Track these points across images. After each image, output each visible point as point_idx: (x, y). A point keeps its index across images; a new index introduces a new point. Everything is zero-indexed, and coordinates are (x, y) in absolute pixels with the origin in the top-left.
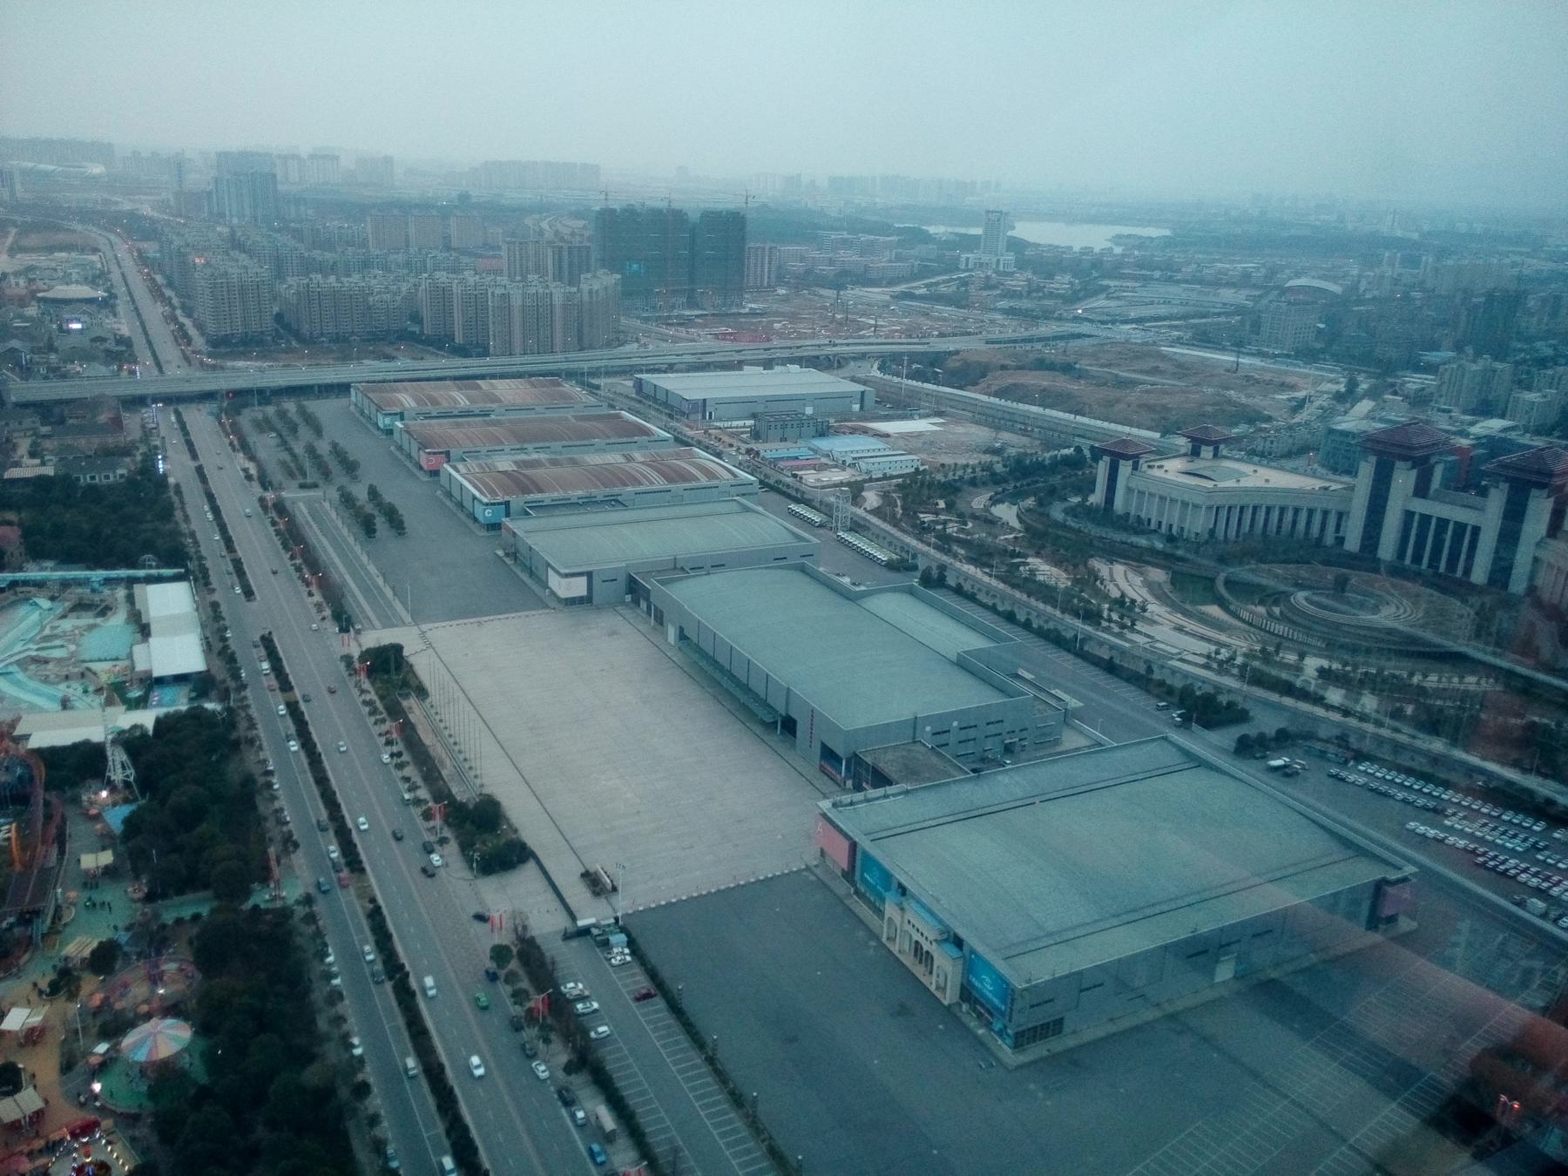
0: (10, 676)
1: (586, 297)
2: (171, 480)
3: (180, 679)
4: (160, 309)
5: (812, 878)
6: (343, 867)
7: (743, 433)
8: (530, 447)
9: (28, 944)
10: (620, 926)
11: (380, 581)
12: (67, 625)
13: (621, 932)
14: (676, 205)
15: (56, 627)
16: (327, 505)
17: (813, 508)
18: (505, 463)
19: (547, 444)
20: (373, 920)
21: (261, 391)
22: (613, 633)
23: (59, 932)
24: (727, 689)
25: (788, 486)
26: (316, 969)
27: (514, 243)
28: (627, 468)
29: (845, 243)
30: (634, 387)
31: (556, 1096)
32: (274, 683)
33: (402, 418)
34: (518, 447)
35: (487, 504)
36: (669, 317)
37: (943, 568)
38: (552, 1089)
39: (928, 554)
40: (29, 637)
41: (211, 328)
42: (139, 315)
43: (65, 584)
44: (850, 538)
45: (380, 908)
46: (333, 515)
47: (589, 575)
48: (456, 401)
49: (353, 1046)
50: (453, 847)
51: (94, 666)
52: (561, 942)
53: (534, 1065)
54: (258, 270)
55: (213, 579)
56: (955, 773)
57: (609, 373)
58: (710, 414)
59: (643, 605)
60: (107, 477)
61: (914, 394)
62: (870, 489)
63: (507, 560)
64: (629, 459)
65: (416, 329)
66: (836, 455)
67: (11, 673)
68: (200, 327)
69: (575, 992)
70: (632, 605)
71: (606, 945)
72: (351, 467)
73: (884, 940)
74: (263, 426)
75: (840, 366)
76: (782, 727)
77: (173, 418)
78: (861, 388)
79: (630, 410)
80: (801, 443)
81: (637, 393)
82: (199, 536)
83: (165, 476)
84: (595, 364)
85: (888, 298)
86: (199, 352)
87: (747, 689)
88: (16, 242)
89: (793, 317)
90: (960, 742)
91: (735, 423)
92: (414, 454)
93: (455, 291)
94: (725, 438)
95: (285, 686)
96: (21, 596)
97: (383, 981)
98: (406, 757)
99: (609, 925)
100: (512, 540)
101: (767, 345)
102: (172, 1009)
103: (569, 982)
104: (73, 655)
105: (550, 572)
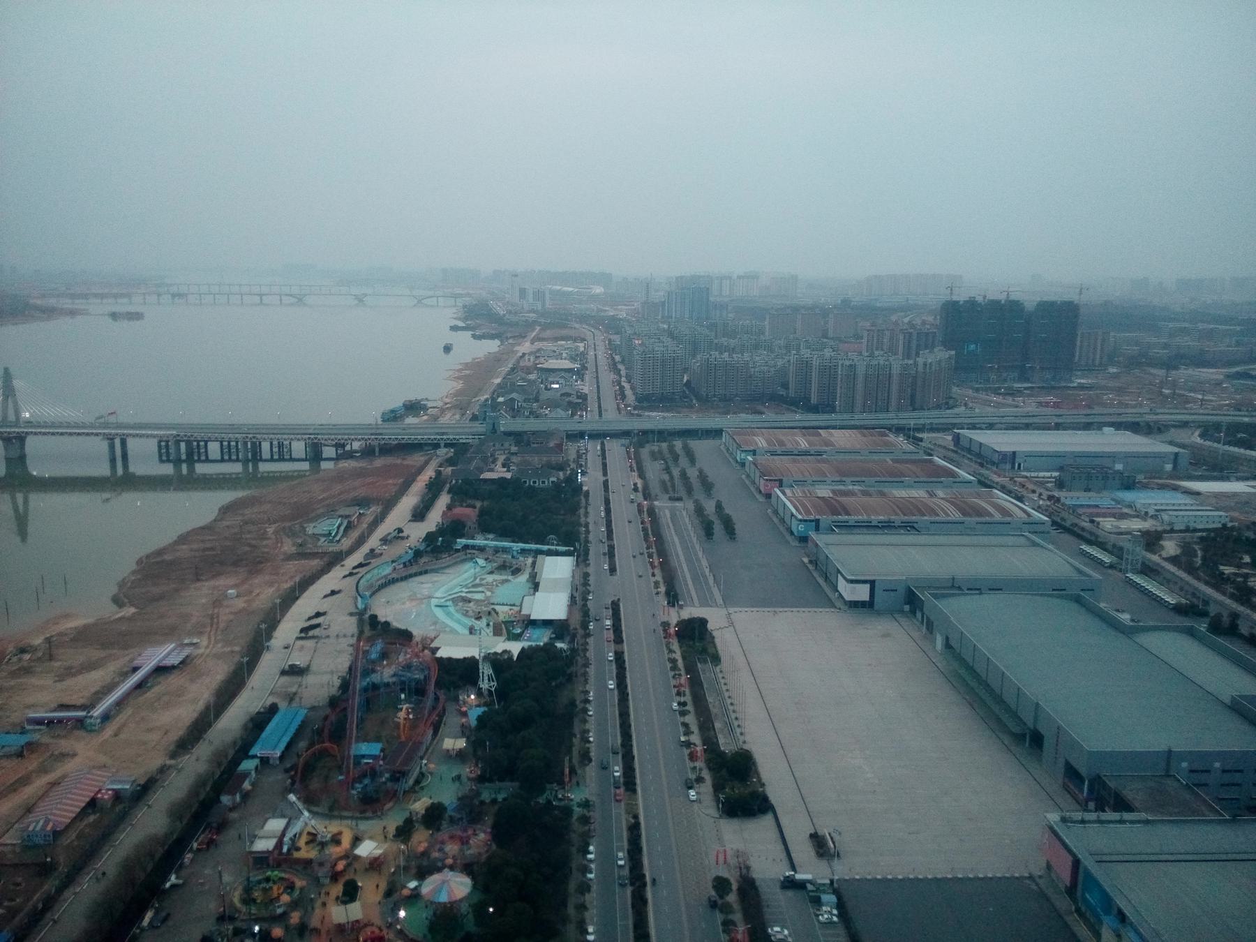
0: (445, 608)
1: (920, 368)
2: (585, 488)
3: (547, 623)
4: (613, 376)
6: (622, 786)
7: (1048, 482)
8: (848, 480)
9: (393, 796)
10: (835, 888)
11: (707, 571)
12: (490, 578)
16: (684, 513)
17: (1105, 550)
18: (824, 492)
19: (863, 479)
20: (632, 833)
21: (660, 432)
23: (415, 792)
24: (973, 689)
25: (1083, 529)
27: (873, 331)
29: (1184, 331)
30: (953, 440)
33: (754, 454)
35: (801, 520)
36: (1000, 388)
37: (1235, 616)
39: (1223, 602)
40: (464, 584)
41: (639, 391)
42: (598, 382)
43: (497, 550)
44: (1138, 579)
46: (687, 520)
47: (872, 583)
48: (797, 443)
49: (588, 933)
50: (707, 787)
56: (1207, 813)
57: (933, 429)
58: (1019, 465)
59: (919, 615)
60: (543, 482)
61: (1235, 459)
62: (1170, 539)
64: (932, 495)
65: (783, 392)
66: (1138, 506)
67: (447, 606)
68: (633, 388)
71: (817, 902)
72: (707, 486)
74: (655, 456)
75: (1160, 431)
77: (599, 448)
78: (1176, 450)
79: (945, 458)
80: (1105, 493)
81: (955, 446)
82: (591, 528)
83: (581, 485)
84: (922, 421)
85: (1222, 377)
87: (1000, 700)
88: (538, 334)
89: (1120, 391)
90: (1222, 785)
91: (1041, 474)
92: (757, 480)
94: (1031, 487)
95: (618, 639)
96: (469, 556)
98: (690, 707)
99: (824, 885)
100: (815, 550)
101: (1089, 412)
102: (468, 868)
103: (777, 926)
104: (487, 598)
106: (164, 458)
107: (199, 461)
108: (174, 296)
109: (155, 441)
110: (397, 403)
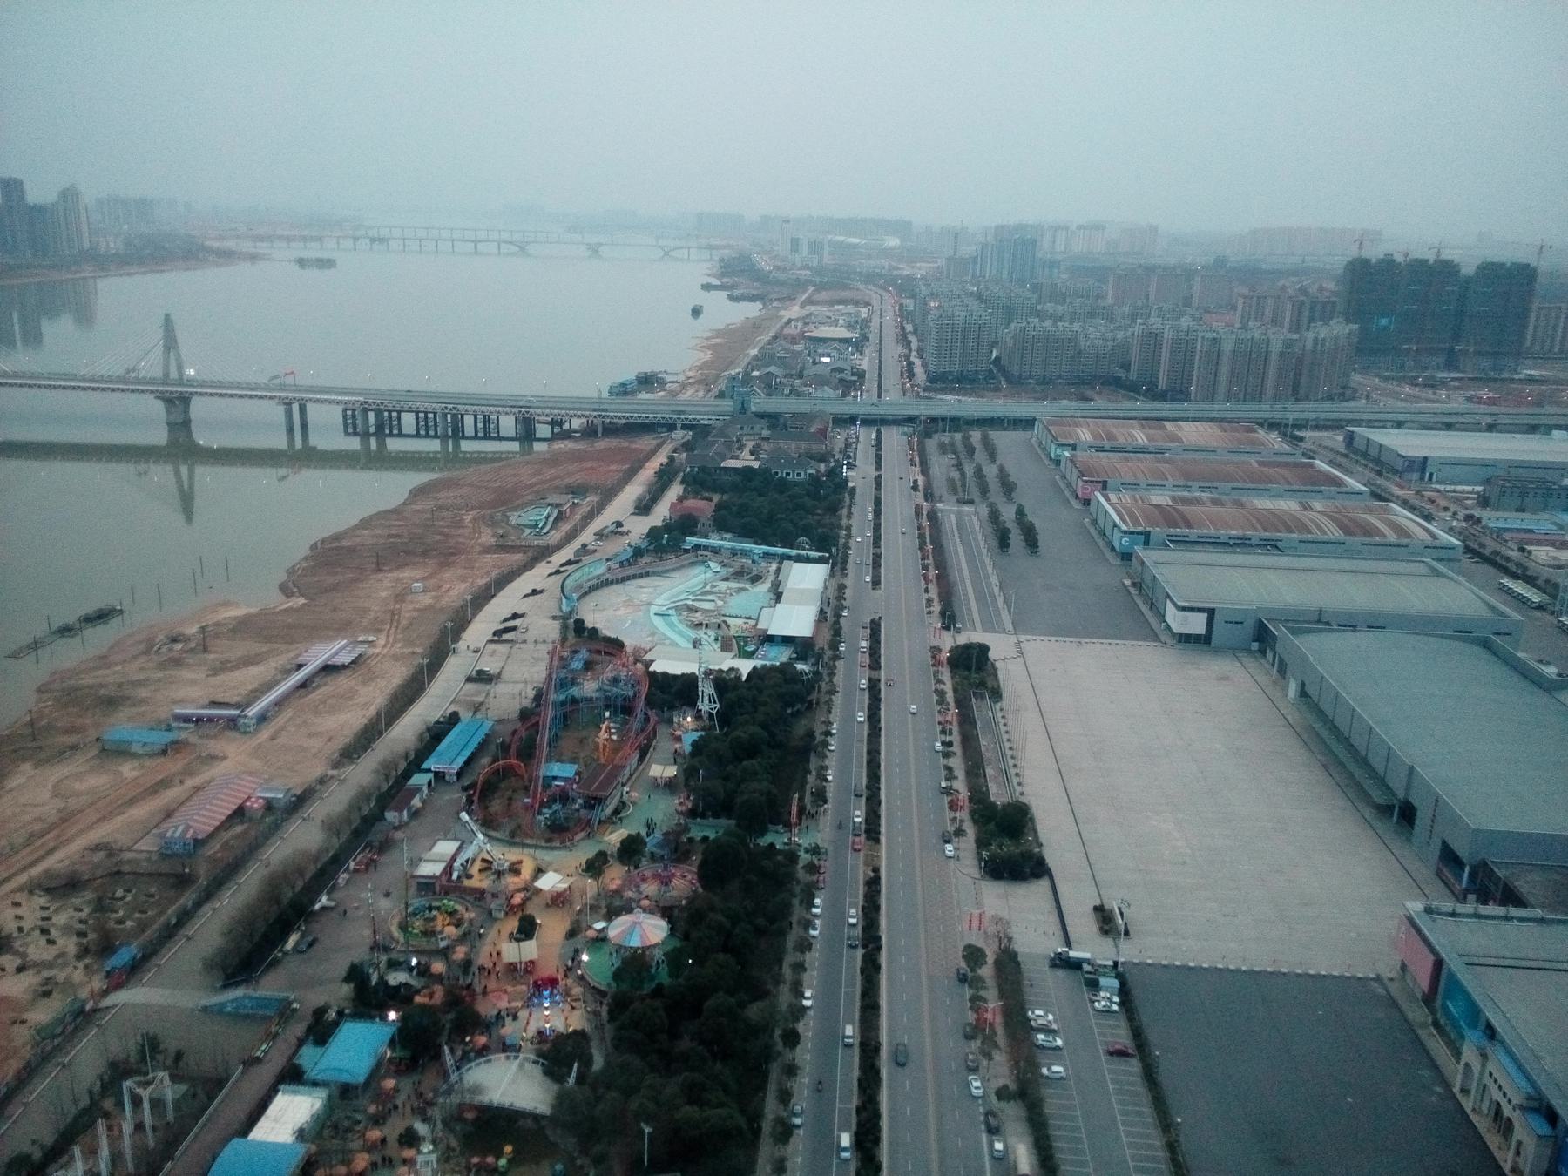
2: (851, 484)
3: (787, 640)
4: (901, 349)
5: (1380, 991)
7: (1468, 498)
8: (1195, 485)
12: (723, 585)
13: (1116, 978)
14: (1446, 255)
15: (715, 586)
18: (1160, 498)
19: (1215, 484)
20: (869, 888)
22: (1224, 678)
25: (1508, 559)
26: (797, 912)
28: (1303, 519)
31: (982, 1118)
32: (866, 660)
34: (1182, 484)
35: (1125, 532)
38: (981, 1109)
43: (734, 553)
45: (879, 878)
48: (1135, 439)
49: (802, 996)
51: (729, 620)
52: (1047, 968)
53: (970, 1078)
54: (984, 314)
55: (850, 566)
58: (1431, 475)
59: (1270, 655)
60: (799, 475)
63: (1132, 590)
64: (1307, 507)
68: (924, 365)
69: (1041, 1021)
70: (1258, 655)
71: (1094, 985)
72: (1008, 488)
73: (1456, 1090)
74: (943, 449)
76: (1399, 814)
77: (873, 436)
86: (918, 386)
87: (1364, 763)
91: (1459, 488)
93: (1166, 335)
94: (1443, 503)
95: (875, 664)
97: (856, 947)
102: (666, 912)
105: (1168, 602)
106: (350, 430)
107: (391, 435)
108: (373, 240)
109: (340, 409)
110: (629, 375)
